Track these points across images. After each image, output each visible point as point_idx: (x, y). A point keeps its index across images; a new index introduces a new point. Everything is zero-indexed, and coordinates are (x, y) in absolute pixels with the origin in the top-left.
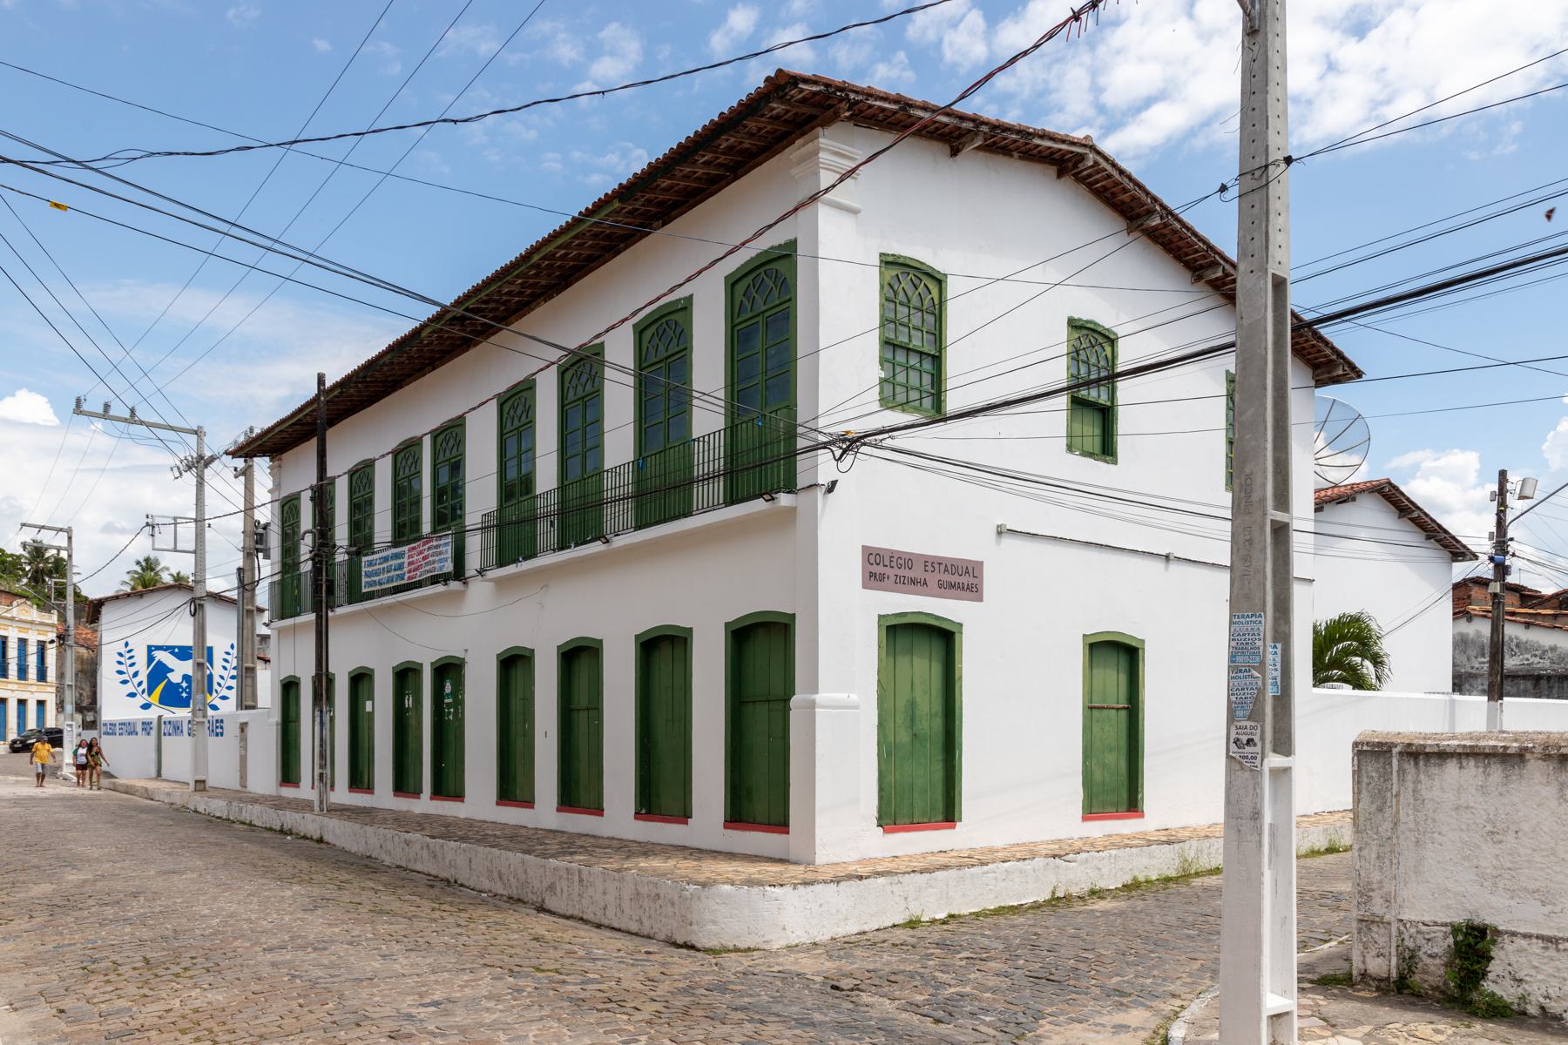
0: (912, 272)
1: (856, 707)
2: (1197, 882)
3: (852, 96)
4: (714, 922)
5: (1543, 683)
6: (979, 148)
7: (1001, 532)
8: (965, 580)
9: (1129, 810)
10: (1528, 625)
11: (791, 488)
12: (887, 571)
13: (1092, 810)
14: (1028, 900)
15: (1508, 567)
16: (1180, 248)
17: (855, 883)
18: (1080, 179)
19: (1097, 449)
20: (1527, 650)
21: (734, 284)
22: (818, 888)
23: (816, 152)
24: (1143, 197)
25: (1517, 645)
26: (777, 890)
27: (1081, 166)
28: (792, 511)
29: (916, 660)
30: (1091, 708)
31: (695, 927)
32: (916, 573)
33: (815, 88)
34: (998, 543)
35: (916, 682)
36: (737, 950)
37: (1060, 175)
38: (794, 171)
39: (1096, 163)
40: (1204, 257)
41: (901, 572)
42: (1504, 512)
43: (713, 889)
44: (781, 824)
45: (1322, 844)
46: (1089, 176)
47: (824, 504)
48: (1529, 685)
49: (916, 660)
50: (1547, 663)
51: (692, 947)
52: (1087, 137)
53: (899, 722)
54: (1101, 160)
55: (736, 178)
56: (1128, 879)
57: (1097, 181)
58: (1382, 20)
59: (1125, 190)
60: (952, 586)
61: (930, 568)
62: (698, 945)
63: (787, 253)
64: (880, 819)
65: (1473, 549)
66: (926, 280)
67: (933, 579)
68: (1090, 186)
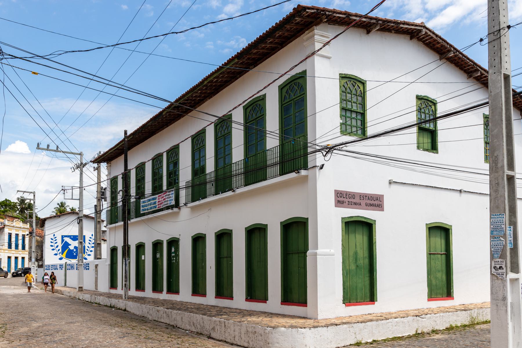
1: (333, 255)
2: (478, 327)
3: (327, 13)
4: (278, 343)
6: (378, 30)
8: (376, 202)
9: (447, 297)
11: (306, 168)
12: (345, 200)
13: (432, 296)
14: (406, 334)
16: (462, 65)
18: (419, 39)
21: (282, 89)
26: (303, 330)
27: (420, 35)
28: (306, 177)
29: (357, 236)
31: (270, 345)
32: (357, 200)
33: (312, 11)
35: (357, 244)
37: (411, 38)
38: (305, 44)
39: (426, 33)
40: (472, 68)
41: (350, 200)
44: (304, 303)
46: (423, 38)
47: (319, 174)
49: (357, 236)
54: (428, 32)
55: (282, 47)
56: (448, 326)
57: (427, 40)
59: (438, 43)
63: (303, 75)
66: (358, 83)
67: (363, 202)
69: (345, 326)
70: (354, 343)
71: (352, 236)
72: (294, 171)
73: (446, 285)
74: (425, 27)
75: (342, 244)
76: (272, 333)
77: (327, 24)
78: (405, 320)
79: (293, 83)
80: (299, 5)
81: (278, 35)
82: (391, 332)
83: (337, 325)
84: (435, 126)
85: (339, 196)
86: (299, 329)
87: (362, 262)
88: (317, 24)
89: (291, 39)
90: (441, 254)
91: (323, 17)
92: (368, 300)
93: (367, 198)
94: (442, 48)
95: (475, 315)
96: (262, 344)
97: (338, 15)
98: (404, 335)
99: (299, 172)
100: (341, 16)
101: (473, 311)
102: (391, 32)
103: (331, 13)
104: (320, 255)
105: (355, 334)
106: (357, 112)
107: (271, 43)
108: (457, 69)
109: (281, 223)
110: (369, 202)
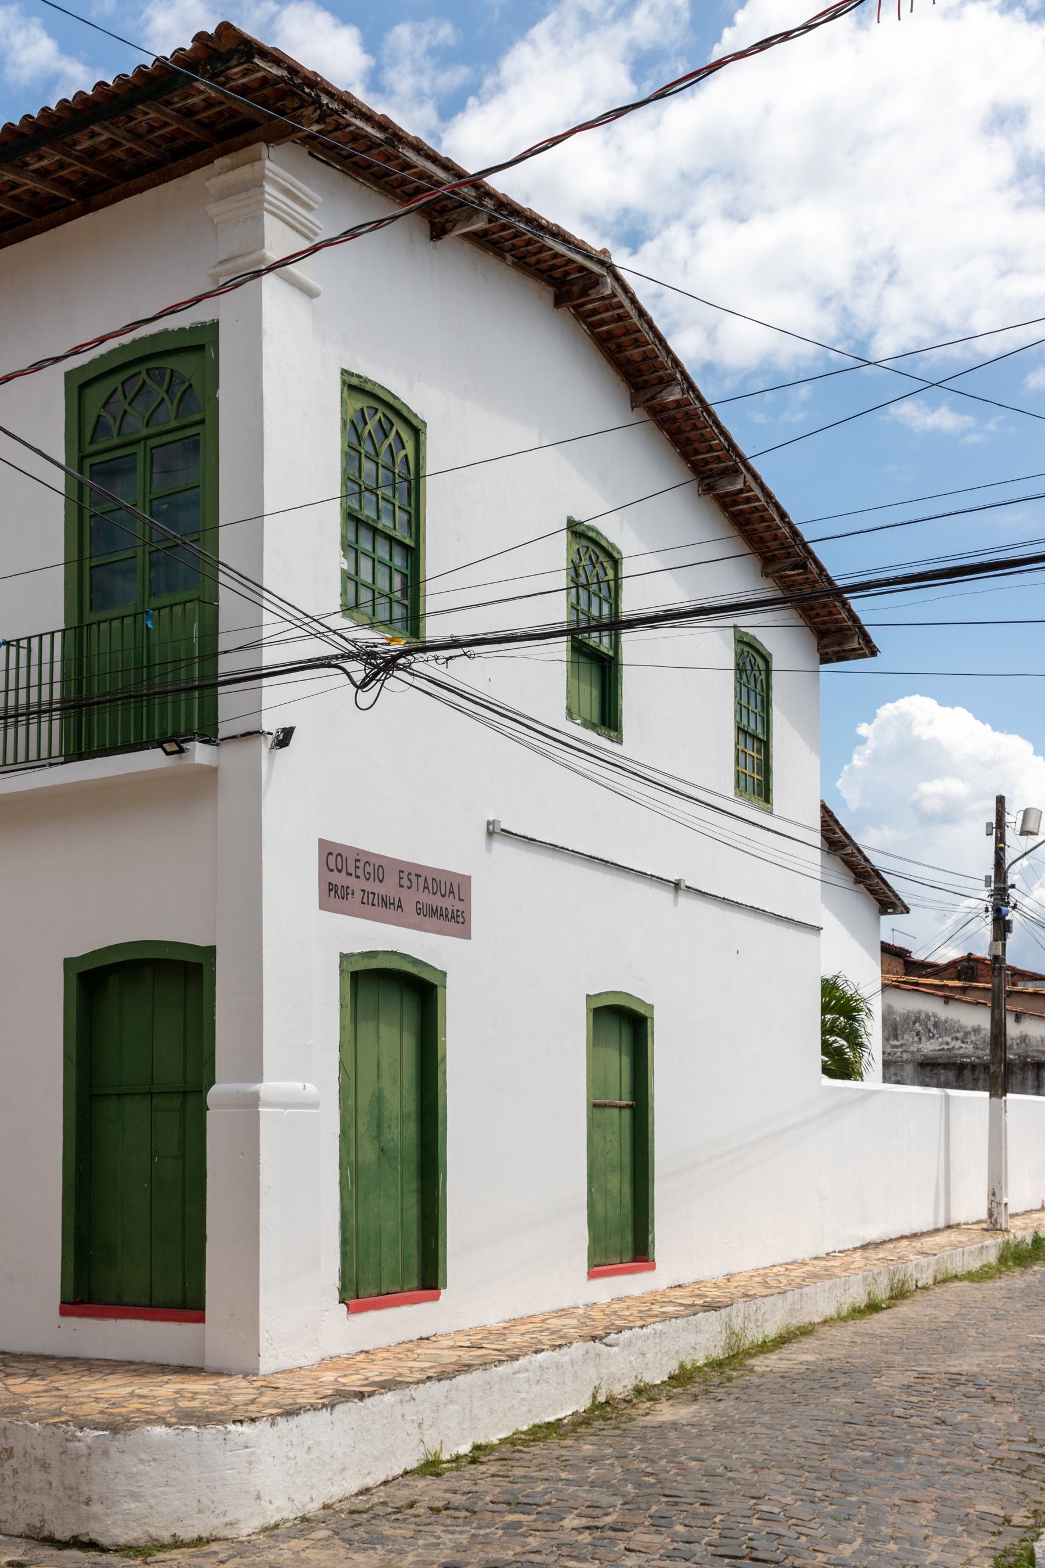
0: (382, 409)
1: (315, 1105)
2: (760, 1363)
3: (325, 100)
4: (135, 1496)
5: (967, 1073)
6: (466, 236)
7: (493, 831)
8: (448, 903)
9: (635, 1260)
10: (947, 1000)
11: (209, 736)
12: (351, 882)
13: (600, 1263)
14: (564, 1412)
15: (1009, 922)
16: (689, 442)
17: (355, 1405)
18: (582, 316)
19: (596, 719)
20: (947, 1031)
21: (83, 387)
22: (305, 1418)
23: (257, 183)
24: (663, 357)
25: (936, 1025)
26: (246, 1429)
27: (593, 294)
28: (211, 773)
29: (384, 1030)
30: (595, 1105)
31: (96, 1508)
32: (388, 889)
33: (276, 71)
34: (489, 849)
35: (384, 1064)
36: (177, 1544)
37: (558, 302)
38: (213, 209)
39: (614, 295)
40: (719, 459)
41: (369, 886)
42: (1002, 849)
43: (134, 1435)
44: (189, 1305)
45: (862, 1300)
46: (594, 312)
47: (271, 767)
48: (951, 1075)
49: (384, 1030)
50: (969, 1049)
51: (92, 1545)
52: (604, 252)
53: (361, 1128)
54: (619, 291)
55: (88, 209)
56: (673, 1367)
57: (604, 322)
58: (659, 232)
59: (637, 343)
60: (434, 912)
61: (405, 882)
62: (104, 1541)
63: (202, 343)
64: (343, 1290)
65: (906, 901)
66: (399, 426)
67: (409, 898)
68: (592, 326)
69: (389, 1397)
70: (415, 1465)
71: (366, 1029)
72: (160, 745)
73: (630, 1220)
74: (611, 269)
75: (341, 1062)
76: (106, 1453)
77: (304, 151)
78: (562, 1356)
79: (142, 368)
80: (225, 28)
81: (85, 144)
82: (524, 1409)
83: (361, 1396)
84: (616, 645)
85: (332, 866)
86: (231, 1427)
87: (396, 1132)
88: (276, 136)
89: (138, 181)
90: (621, 1108)
91: (307, 112)
92: (415, 1283)
93: (421, 881)
94: (643, 366)
95: (737, 1324)
96: (50, 1505)
97: (358, 122)
98: (560, 1416)
99: (181, 751)
100: (369, 129)
101: (733, 1311)
102: (504, 259)
103: (334, 106)
104: (271, 1105)
105: (420, 1425)
106: (391, 540)
107: (42, 174)
108: (673, 453)
109: (67, 961)
110: (426, 898)
